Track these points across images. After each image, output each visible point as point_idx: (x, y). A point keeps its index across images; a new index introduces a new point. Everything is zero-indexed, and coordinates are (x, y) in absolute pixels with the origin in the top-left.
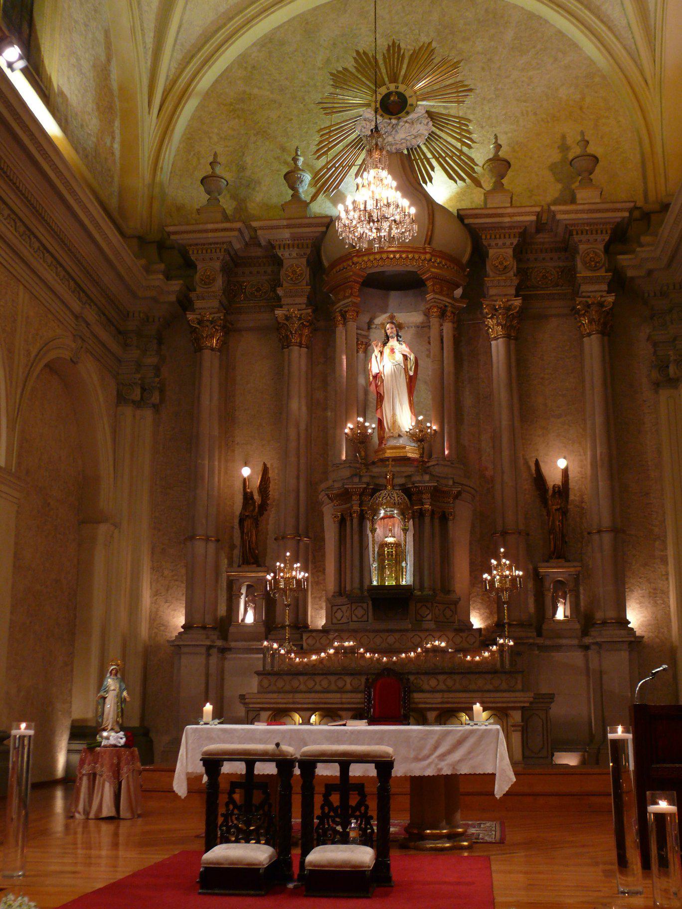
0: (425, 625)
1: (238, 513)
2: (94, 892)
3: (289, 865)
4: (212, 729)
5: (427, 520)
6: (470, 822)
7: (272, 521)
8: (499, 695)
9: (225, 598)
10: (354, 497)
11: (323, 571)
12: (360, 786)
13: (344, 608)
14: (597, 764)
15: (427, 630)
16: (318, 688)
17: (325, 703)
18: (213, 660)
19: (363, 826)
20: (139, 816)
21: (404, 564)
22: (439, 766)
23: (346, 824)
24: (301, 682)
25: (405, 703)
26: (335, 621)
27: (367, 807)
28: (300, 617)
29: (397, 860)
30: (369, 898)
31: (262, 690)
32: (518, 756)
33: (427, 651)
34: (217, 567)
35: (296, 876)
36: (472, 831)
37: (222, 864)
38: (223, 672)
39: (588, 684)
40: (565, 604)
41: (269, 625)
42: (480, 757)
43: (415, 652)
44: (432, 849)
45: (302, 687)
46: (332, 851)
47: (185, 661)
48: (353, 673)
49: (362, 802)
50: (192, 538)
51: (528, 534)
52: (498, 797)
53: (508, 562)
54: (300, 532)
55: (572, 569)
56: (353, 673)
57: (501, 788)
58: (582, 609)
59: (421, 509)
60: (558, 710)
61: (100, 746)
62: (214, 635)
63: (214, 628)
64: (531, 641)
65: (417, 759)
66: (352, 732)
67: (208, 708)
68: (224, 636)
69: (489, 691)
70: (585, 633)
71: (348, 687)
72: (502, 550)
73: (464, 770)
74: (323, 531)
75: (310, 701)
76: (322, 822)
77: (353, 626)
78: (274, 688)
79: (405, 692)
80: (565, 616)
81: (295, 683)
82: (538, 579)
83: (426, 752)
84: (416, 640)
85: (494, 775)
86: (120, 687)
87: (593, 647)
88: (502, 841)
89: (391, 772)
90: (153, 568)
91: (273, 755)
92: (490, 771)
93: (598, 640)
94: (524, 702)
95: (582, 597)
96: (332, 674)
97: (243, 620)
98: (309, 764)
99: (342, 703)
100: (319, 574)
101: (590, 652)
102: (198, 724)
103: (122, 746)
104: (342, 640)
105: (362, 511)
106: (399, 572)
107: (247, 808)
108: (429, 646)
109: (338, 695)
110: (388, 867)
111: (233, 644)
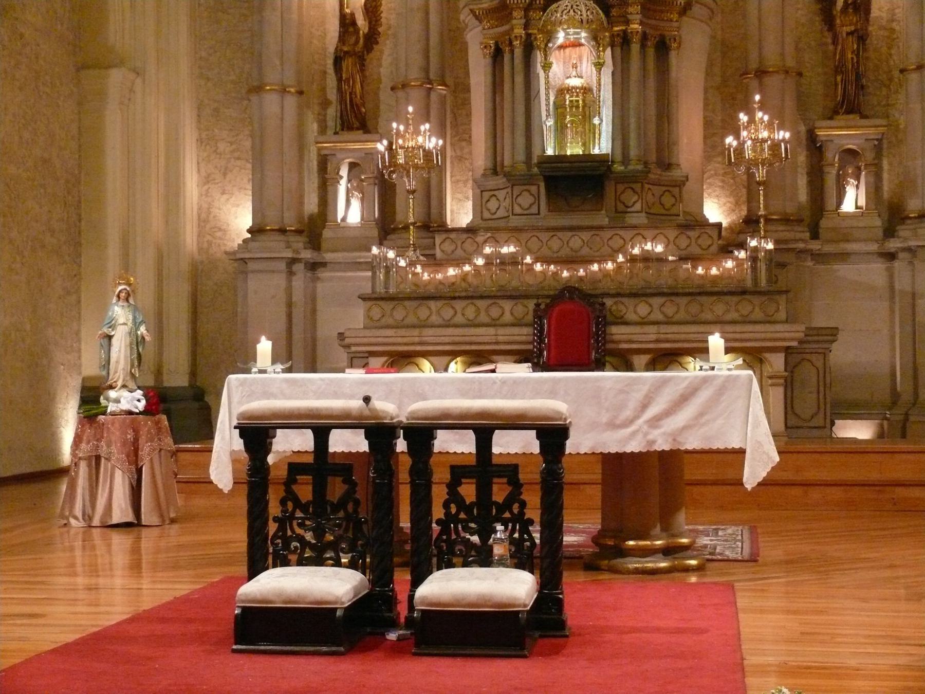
0: (632, 219)
1: (331, 49)
2: (54, 651)
3: (390, 601)
4: (271, 379)
5: (635, 48)
6: (701, 528)
7: (387, 62)
8: (750, 328)
9: (316, 185)
10: (515, 14)
11: (469, 141)
12: (510, 470)
13: (501, 194)
14: (904, 436)
15: (635, 227)
16: (459, 319)
17: (471, 343)
18: (299, 282)
19: (516, 535)
20: (173, 521)
21: (596, 121)
22: (650, 437)
23: (486, 532)
24: (434, 311)
25: (597, 341)
26: (487, 215)
27: (523, 505)
28: (434, 211)
29: (576, 590)
30: (525, 657)
31: (372, 324)
32: (781, 427)
33: (633, 259)
34: (301, 136)
35: (402, 620)
36: (704, 541)
37: (271, 602)
38: (314, 300)
39: (892, 311)
40: (857, 187)
41: (386, 227)
42: (720, 421)
43: (614, 261)
44: (637, 571)
45: (434, 319)
46: (462, 578)
47: (253, 283)
48: (516, 296)
49: (515, 496)
50: (258, 89)
51: (800, 74)
52: (749, 487)
53: (766, 118)
54: (432, 76)
55: (872, 131)
56: (516, 296)
57: (753, 473)
58: (886, 195)
59: (625, 32)
60: (843, 354)
61: (104, 413)
62: (299, 242)
63: (299, 232)
64: (801, 245)
65: (613, 425)
66: (504, 382)
67: (264, 347)
68: (315, 242)
69: (733, 322)
70: (889, 232)
71: (508, 317)
72: (757, 97)
73: (692, 442)
74: (467, 74)
75: (447, 340)
76: (445, 529)
77: (515, 221)
78: (391, 321)
79: (597, 325)
80: (857, 207)
81: (423, 313)
82: (815, 147)
83: (627, 413)
84: (617, 242)
85: (742, 452)
86: (134, 318)
87: (901, 255)
88: (753, 559)
89: (562, 447)
90: (200, 141)
91: (361, 417)
92: (736, 444)
93: (912, 243)
94: (792, 339)
95: (885, 176)
96: (482, 297)
97: (344, 219)
98: (421, 434)
99: (497, 343)
100: (464, 144)
101: (896, 264)
102: (248, 371)
103: (140, 413)
104: (497, 242)
105: (529, 35)
106: (590, 134)
107: (319, 507)
108: (636, 251)
109: (491, 331)
110: (559, 603)
111: (328, 257)
